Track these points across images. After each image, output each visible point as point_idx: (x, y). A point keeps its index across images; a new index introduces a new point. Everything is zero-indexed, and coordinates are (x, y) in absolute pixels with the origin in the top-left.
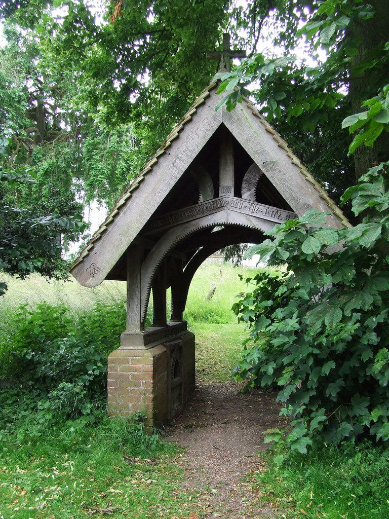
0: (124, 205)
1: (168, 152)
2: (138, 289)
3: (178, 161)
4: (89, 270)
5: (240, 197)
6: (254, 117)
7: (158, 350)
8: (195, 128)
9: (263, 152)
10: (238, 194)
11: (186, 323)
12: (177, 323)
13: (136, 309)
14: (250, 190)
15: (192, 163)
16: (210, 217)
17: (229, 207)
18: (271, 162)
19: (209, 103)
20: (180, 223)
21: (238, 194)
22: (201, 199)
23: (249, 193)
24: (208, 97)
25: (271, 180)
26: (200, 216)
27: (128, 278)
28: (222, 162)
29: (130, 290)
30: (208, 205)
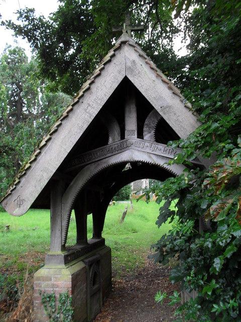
0: (45, 145)
1: (81, 101)
2: (60, 216)
3: (89, 108)
4: (16, 201)
5: (143, 138)
6: (151, 70)
7: (78, 267)
8: (103, 81)
9: (160, 98)
10: (140, 135)
11: (104, 240)
12: (99, 240)
13: (58, 233)
14: (150, 133)
15: (101, 109)
16: (116, 156)
17: (133, 147)
18: (167, 107)
19: (115, 60)
20: (94, 161)
21: (140, 135)
22: (110, 140)
23: (149, 135)
24: (113, 56)
25: (168, 121)
26: (109, 155)
27: (51, 207)
28: (127, 109)
29: (53, 219)
30: (116, 146)
